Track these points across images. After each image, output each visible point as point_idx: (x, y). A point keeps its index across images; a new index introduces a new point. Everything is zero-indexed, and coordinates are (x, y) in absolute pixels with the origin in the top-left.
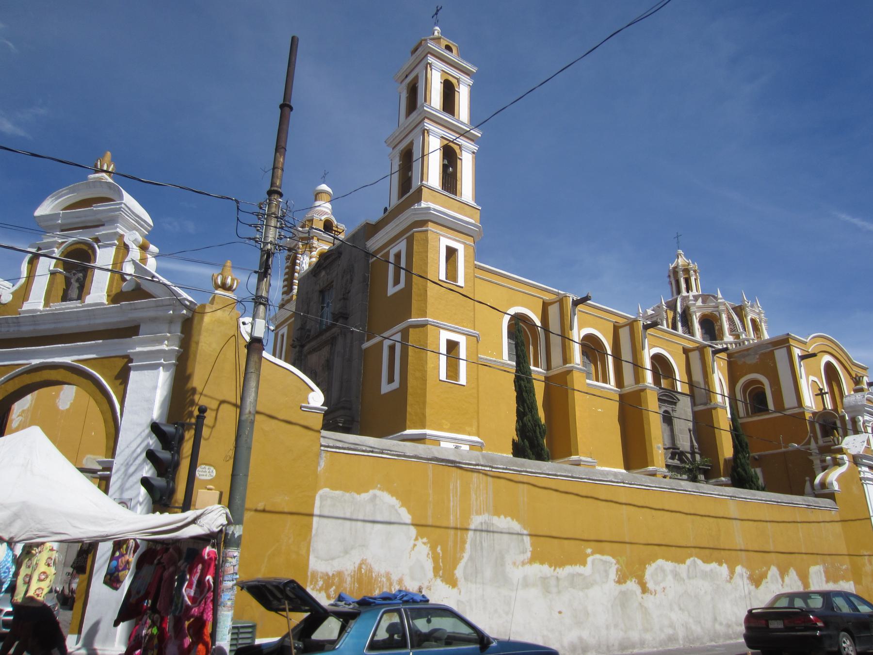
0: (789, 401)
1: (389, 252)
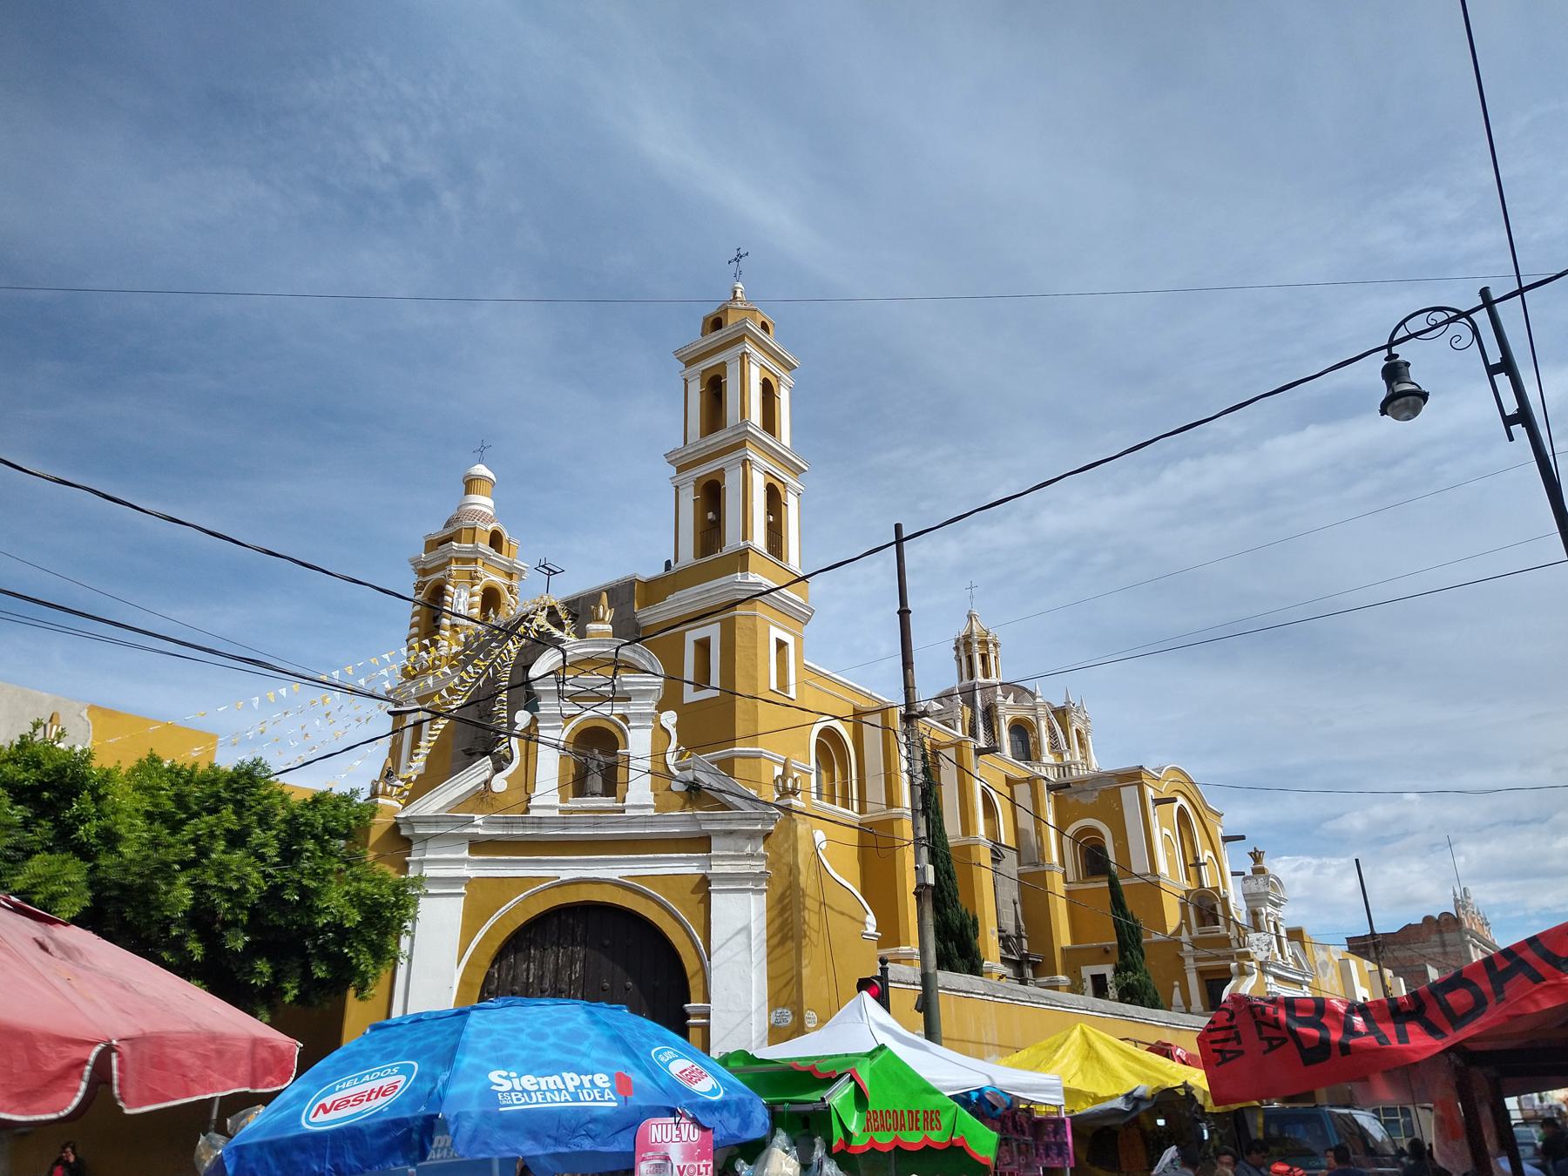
0: (1139, 865)
1: (683, 633)
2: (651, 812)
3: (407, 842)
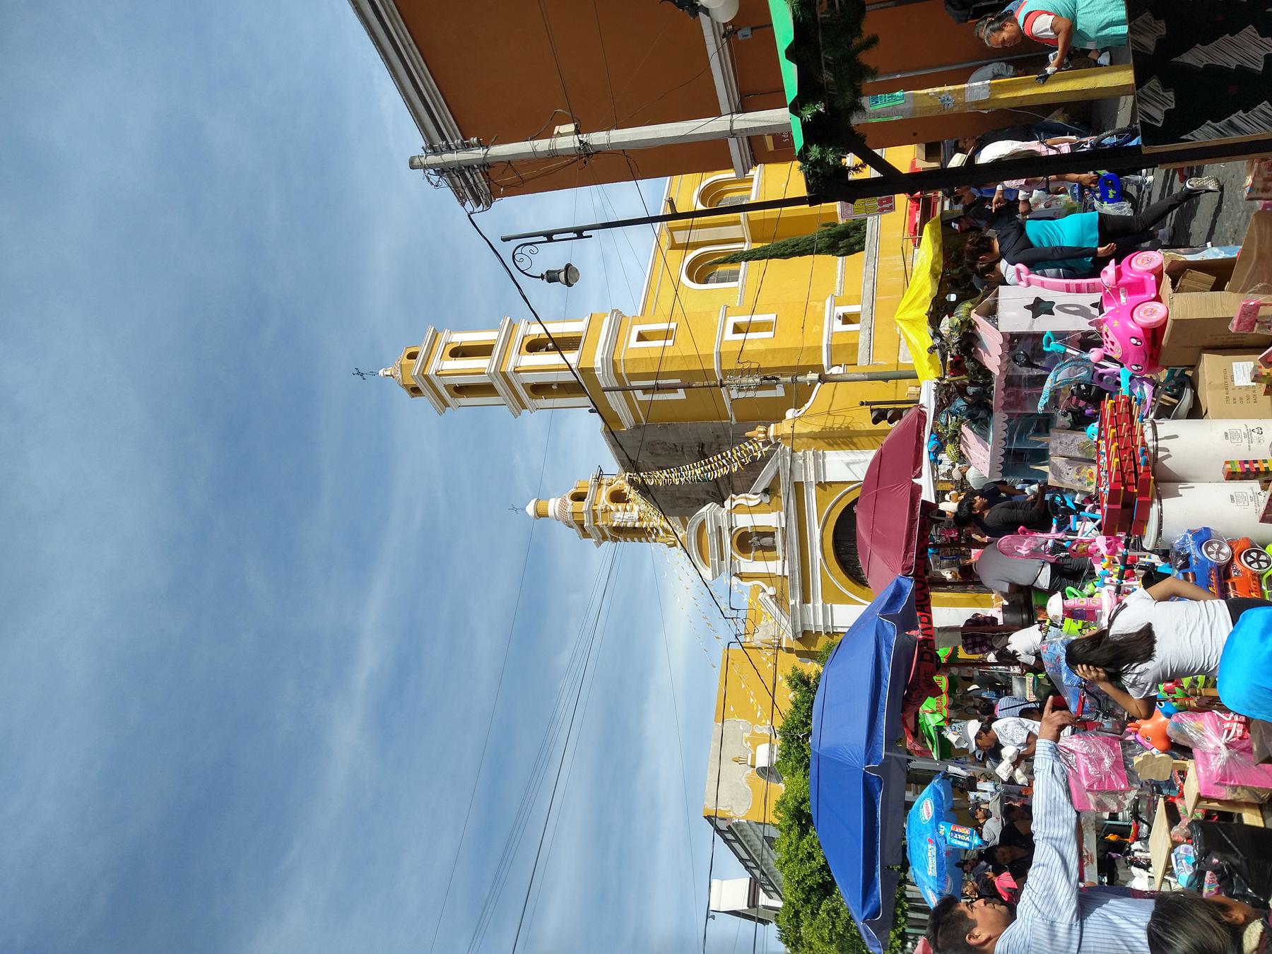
2: (783, 514)
3: (805, 632)
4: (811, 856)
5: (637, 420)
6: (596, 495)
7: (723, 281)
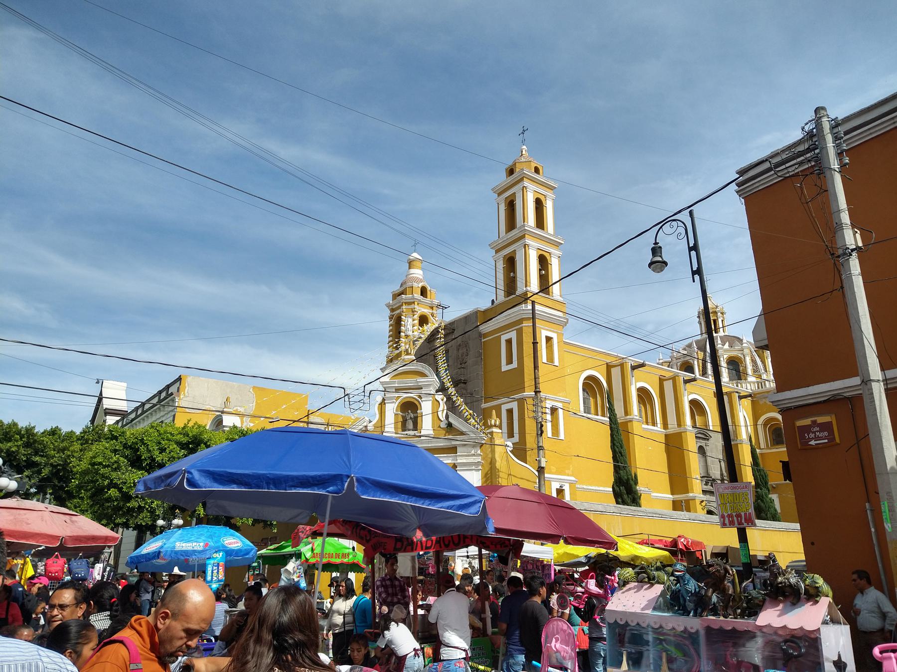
4: (162, 450)
5: (485, 335)
6: (425, 304)
7: (584, 403)
